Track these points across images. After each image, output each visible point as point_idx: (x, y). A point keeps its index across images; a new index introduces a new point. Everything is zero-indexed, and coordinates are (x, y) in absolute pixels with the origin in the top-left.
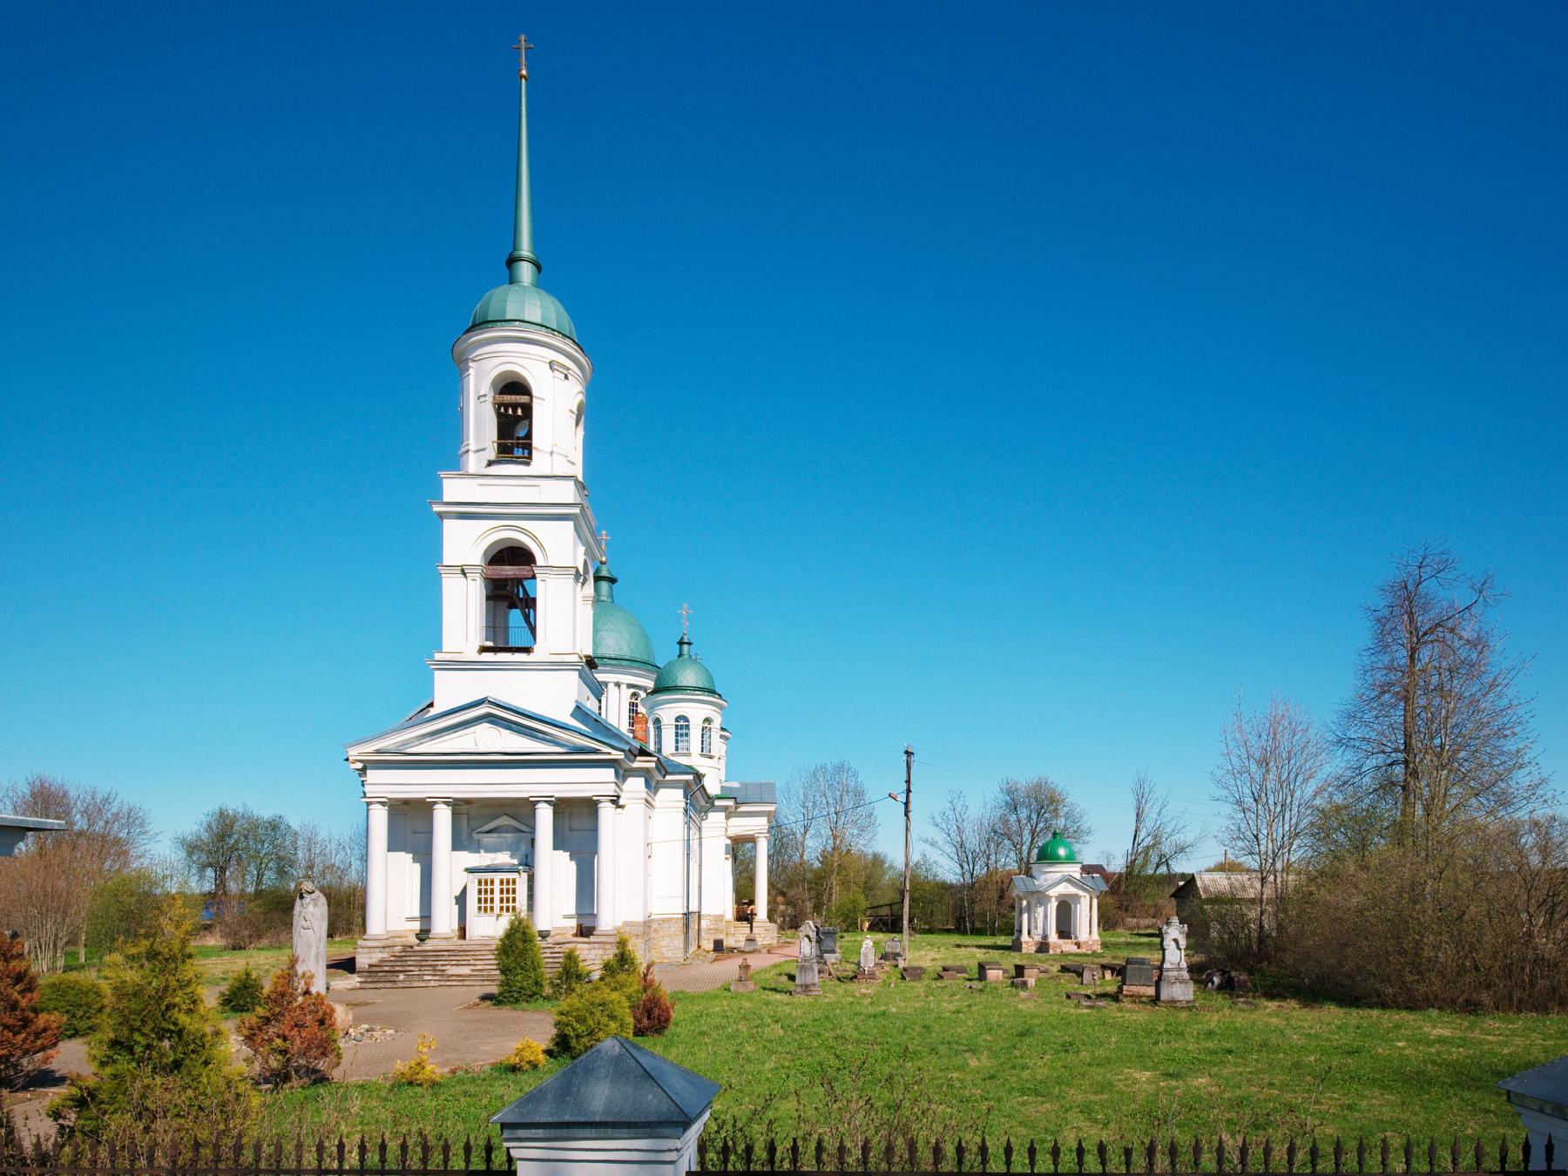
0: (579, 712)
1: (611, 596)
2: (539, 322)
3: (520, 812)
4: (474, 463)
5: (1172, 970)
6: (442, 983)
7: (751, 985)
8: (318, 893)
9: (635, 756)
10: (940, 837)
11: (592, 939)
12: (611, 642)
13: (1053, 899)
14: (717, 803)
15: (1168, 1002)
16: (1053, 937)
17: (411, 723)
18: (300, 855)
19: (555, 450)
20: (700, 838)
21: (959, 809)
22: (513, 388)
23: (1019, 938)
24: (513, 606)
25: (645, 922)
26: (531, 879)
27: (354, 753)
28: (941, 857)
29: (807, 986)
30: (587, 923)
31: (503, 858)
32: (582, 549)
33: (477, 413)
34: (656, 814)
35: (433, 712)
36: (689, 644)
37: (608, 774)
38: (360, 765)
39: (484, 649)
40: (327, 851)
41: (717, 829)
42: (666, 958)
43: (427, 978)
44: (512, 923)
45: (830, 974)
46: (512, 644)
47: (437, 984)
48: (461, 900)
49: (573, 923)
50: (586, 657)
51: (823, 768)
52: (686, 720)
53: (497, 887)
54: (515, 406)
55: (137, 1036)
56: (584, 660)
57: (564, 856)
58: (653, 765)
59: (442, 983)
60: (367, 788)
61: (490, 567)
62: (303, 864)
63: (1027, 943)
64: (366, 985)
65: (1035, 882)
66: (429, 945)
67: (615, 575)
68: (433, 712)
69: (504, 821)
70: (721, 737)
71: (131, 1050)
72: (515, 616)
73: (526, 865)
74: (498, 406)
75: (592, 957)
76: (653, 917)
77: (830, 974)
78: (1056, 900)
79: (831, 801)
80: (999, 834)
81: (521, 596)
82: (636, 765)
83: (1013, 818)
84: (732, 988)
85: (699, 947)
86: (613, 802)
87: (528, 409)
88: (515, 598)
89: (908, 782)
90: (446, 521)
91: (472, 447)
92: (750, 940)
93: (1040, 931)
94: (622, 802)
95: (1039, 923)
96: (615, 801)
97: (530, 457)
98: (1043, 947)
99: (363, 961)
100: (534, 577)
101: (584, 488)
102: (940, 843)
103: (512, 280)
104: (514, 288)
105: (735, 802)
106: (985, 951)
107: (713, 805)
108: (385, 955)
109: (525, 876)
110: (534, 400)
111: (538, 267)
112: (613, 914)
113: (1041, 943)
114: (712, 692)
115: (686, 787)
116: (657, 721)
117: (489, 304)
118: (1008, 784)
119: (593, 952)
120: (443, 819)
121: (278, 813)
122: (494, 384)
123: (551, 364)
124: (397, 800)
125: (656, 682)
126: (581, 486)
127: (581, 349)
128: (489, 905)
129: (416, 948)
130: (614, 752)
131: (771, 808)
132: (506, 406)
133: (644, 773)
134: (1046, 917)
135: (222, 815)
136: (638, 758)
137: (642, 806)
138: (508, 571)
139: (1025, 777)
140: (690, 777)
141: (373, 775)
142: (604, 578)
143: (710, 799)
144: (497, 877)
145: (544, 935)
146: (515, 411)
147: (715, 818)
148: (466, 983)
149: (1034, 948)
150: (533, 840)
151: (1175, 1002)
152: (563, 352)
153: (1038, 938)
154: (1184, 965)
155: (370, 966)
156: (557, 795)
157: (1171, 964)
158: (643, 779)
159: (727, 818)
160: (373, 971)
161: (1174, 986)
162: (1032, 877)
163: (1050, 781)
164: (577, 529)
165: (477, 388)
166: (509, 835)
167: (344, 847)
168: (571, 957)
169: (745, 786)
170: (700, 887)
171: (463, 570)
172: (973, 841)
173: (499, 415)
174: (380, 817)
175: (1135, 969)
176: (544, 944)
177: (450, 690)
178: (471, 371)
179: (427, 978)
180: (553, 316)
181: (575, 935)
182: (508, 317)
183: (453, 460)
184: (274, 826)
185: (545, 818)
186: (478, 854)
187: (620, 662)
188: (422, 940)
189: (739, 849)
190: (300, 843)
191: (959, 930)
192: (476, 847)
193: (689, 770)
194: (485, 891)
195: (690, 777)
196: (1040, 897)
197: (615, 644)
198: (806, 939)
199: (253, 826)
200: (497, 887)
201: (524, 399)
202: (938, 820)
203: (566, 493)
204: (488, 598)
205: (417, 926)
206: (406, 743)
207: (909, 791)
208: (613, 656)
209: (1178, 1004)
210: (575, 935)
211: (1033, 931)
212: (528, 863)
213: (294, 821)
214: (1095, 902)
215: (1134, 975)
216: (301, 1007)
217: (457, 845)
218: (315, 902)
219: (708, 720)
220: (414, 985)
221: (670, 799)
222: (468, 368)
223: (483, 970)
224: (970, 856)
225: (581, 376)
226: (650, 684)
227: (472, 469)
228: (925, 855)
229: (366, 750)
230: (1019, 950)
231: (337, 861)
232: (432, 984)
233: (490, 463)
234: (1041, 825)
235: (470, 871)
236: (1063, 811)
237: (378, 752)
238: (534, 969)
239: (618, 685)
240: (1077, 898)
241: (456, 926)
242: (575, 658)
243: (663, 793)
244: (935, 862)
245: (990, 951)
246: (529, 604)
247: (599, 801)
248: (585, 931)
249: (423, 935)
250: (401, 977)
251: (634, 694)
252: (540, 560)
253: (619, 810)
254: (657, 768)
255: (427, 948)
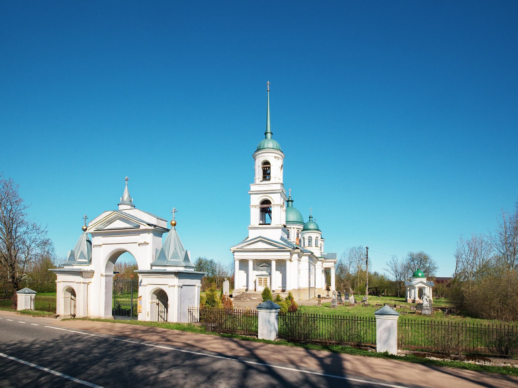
0: (282, 239)
1: (292, 205)
2: (272, 147)
3: (267, 263)
4: (258, 181)
5: (425, 306)
6: (251, 301)
7: (321, 305)
8: (227, 280)
9: (295, 249)
10: (390, 269)
11: (285, 293)
12: (292, 217)
13: (417, 288)
14: (319, 259)
15: (424, 314)
16: (417, 299)
17: (244, 242)
18: (217, 269)
19: (276, 177)
20: (315, 269)
21: (395, 260)
22: (266, 163)
23: (407, 299)
24: (266, 213)
25: (298, 289)
26: (271, 278)
27: (232, 249)
28: (390, 274)
29: (334, 306)
30: (284, 289)
31: (265, 273)
32: (282, 199)
33: (258, 170)
34: (301, 263)
35: (249, 239)
36: (312, 217)
37: (289, 254)
38: (233, 251)
39: (260, 224)
40: (223, 268)
41: (319, 267)
42: (304, 298)
43: (247, 299)
44: (265, 288)
45: (343, 304)
46: (266, 223)
47: (250, 301)
48: (255, 282)
49: (281, 289)
50: (284, 225)
51: (355, 248)
52: (311, 237)
53: (263, 280)
54: (266, 168)
55: (210, 301)
56: (283, 226)
57: (278, 272)
58: (300, 251)
59: (251, 301)
60: (235, 257)
61: (261, 205)
62: (218, 271)
63: (409, 300)
64: (235, 300)
65: (412, 283)
66: (248, 292)
67: (293, 200)
68: (249, 239)
69: (264, 264)
70: (322, 240)
71: (208, 303)
72: (267, 215)
73: (270, 275)
74: (263, 168)
75: (284, 296)
76: (301, 288)
77: (343, 304)
78: (418, 288)
79: (357, 257)
80: (407, 268)
81: (268, 210)
82: (295, 251)
83: (412, 263)
84: (316, 306)
85: (315, 297)
86: (290, 260)
87: (269, 168)
88: (267, 211)
89: (367, 255)
90: (251, 195)
91: (257, 178)
92: (328, 295)
93: (413, 297)
94: (292, 260)
95: (413, 295)
96: (291, 260)
97: (270, 179)
98: (414, 301)
99: (234, 295)
100: (271, 207)
101: (283, 184)
102: (390, 270)
103: (266, 138)
104: (266, 140)
105: (325, 258)
106: (395, 301)
107: (318, 259)
108: (239, 294)
109: (269, 277)
110: (271, 166)
111: (272, 134)
112: (289, 287)
113: (414, 300)
114: (318, 230)
115: (309, 256)
116: (304, 238)
117: (260, 145)
118: (410, 253)
119: (285, 296)
120: (251, 264)
121: (212, 259)
122: (262, 163)
123: (275, 157)
124: (241, 259)
125: (304, 227)
126: (282, 184)
127: (282, 152)
128: (261, 284)
129: (245, 293)
130: (290, 248)
131: (335, 260)
132: (265, 168)
133: (298, 253)
134: (415, 293)
135: (200, 259)
136: (296, 250)
137: (297, 261)
138: (265, 206)
139: (416, 251)
140: (310, 254)
141: (236, 254)
142: (290, 201)
143: (317, 258)
144: (263, 277)
145: (273, 291)
146: (267, 169)
147: (319, 263)
148: (256, 301)
149: (411, 302)
150: (271, 269)
151: (425, 314)
152: (279, 154)
153: (413, 299)
154: (428, 305)
155: (236, 296)
156: (276, 259)
157: (425, 305)
158: (297, 255)
159: (322, 263)
160: (236, 297)
161: (425, 310)
162: (411, 281)
163: (424, 252)
164: (281, 195)
165: (258, 164)
166: (266, 267)
167: (227, 268)
168: (278, 296)
169: (328, 254)
170: (315, 281)
171: (255, 206)
172: (400, 270)
173: (263, 170)
174: (237, 263)
175: (419, 306)
176: (273, 293)
177: (253, 234)
178: (257, 160)
179: (247, 299)
180: (275, 145)
181: (281, 292)
182: (265, 147)
183: (252, 181)
184: (211, 262)
185: (274, 264)
186: (258, 272)
187: (294, 222)
188: (246, 291)
189: (327, 272)
190: (217, 266)
191: (396, 296)
192: (258, 270)
193: (310, 252)
194: (260, 281)
195: (310, 254)
196: (413, 287)
197: (293, 217)
198: (334, 295)
199: (206, 262)
200: (263, 280)
201: (269, 166)
202: (389, 263)
203: (278, 187)
204: (261, 211)
205: (245, 288)
206: (243, 247)
207: (367, 258)
208: (292, 221)
209: (426, 315)
210: (281, 292)
211: (411, 297)
212: (270, 274)
213: (216, 261)
214: (431, 289)
215: (419, 308)
216: (227, 301)
217: (254, 269)
218: (227, 282)
219: (317, 237)
220: (245, 301)
221: (305, 259)
222: (256, 160)
223: (259, 298)
224: (399, 274)
225: (282, 158)
226: (302, 228)
227: (257, 183)
228: (385, 274)
229: (234, 248)
230: (407, 302)
231: (225, 271)
232: (249, 301)
233: (261, 181)
234: (422, 266)
235: (257, 276)
236: (428, 261)
237: (237, 248)
238: (270, 298)
239: (294, 228)
240: (424, 288)
241: (254, 288)
242: (281, 226)
243: (303, 258)
244: (388, 276)
245: (396, 301)
246: (270, 212)
247: (286, 260)
248: (283, 291)
249: (247, 290)
250: (242, 299)
251: (298, 230)
252: (272, 203)
253: (291, 262)
254: (301, 252)
255: (248, 293)
